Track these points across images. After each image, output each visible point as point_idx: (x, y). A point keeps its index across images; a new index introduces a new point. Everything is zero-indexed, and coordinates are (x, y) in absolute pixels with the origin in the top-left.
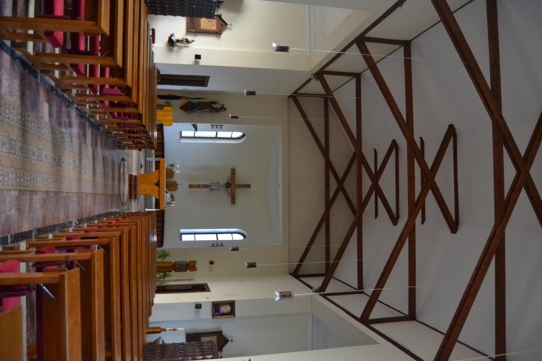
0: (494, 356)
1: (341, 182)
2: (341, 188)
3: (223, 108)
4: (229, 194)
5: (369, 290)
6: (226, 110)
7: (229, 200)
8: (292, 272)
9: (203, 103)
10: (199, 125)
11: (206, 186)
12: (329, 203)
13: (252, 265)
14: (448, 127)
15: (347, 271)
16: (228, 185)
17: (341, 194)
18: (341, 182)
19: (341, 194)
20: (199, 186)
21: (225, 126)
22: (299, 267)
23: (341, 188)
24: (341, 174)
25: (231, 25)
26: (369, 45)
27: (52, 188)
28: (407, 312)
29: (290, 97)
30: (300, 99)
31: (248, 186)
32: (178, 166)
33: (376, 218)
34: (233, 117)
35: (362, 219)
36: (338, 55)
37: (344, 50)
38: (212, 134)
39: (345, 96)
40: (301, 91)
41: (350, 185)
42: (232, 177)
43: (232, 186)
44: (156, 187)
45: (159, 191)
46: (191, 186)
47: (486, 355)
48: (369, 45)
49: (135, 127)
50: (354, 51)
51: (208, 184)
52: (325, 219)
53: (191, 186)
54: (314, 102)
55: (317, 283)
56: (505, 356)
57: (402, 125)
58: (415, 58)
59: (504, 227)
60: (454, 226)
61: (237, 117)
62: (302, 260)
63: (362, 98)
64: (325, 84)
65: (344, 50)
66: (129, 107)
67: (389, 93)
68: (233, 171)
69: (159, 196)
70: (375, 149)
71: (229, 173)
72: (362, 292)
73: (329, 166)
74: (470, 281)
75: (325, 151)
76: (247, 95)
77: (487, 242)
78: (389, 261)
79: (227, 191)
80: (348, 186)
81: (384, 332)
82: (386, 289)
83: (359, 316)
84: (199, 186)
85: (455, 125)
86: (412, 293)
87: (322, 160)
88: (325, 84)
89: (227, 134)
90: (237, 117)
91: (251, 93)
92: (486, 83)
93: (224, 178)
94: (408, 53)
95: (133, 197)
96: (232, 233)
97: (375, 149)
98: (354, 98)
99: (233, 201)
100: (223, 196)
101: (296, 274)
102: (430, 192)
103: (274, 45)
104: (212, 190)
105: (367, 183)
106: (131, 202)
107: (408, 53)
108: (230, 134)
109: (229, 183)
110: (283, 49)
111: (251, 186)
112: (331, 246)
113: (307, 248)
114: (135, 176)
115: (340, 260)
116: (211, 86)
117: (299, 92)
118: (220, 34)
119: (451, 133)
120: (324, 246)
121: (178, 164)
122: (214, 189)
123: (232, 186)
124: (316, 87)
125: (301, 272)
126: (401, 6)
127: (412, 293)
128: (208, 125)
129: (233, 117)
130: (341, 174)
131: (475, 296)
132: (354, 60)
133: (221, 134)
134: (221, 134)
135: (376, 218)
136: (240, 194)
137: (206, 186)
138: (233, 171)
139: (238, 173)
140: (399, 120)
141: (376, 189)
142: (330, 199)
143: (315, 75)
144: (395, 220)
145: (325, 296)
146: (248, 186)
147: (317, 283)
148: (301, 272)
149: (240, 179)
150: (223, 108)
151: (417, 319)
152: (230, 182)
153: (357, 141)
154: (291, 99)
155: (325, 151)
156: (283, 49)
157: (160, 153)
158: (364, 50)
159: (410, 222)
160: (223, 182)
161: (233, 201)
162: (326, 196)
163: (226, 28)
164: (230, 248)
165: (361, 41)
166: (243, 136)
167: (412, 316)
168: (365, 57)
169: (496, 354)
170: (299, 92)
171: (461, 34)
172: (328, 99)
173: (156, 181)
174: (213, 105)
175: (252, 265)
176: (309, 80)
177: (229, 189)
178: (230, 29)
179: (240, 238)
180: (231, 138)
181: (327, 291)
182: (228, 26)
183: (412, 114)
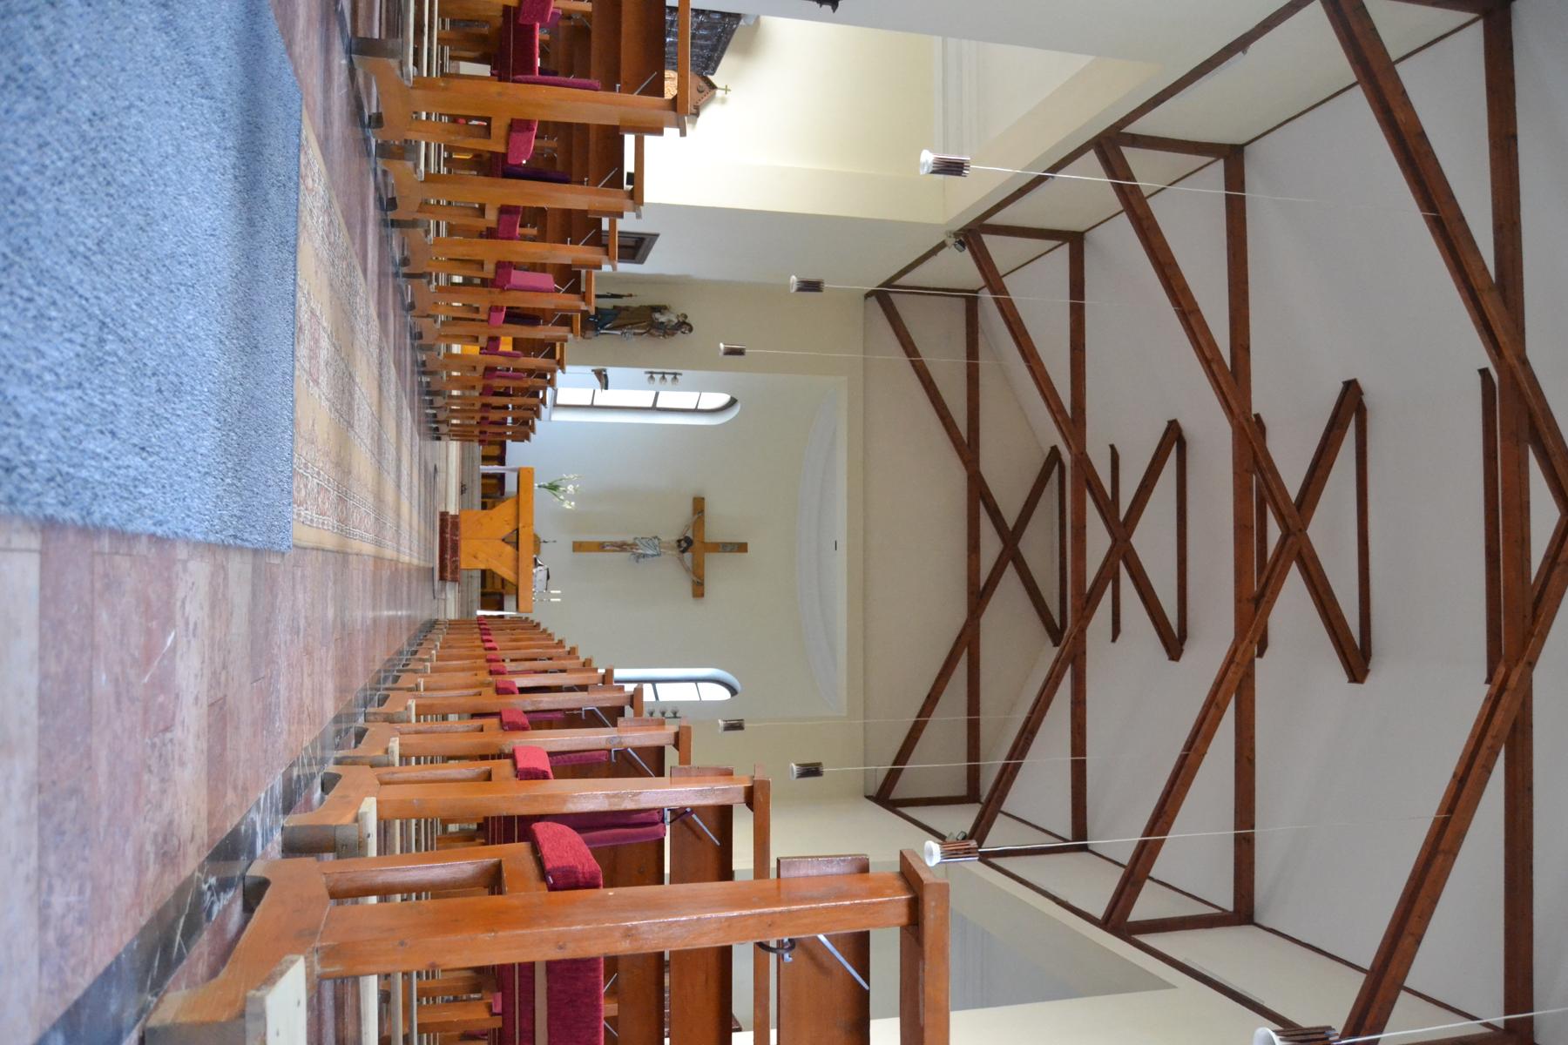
0: (1499, 1019)
1: (1011, 538)
2: (1011, 554)
3: (683, 325)
4: (687, 570)
5: (1118, 836)
6: (691, 330)
7: (687, 587)
8: (873, 791)
9: (627, 309)
10: (612, 372)
11: (622, 547)
12: (979, 597)
13: (811, 771)
14: (1340, 386)
15: (1040, 792)
16: (685, 544)
17: (1010, 571)
18: (1011, 538)
19: (1010, 571)
20: (601, 547)
21: (687, 375)
22: (893, 777)
23: (1011, 554)
24: (1011, 519)
25: (726, 90)
26: (1132, 155)
27: (329, 540)
28: (1229, 905)
29: (868, 295)
30: (900, 302)
31: (742, 547)
32: (570, 488)
33: (1114, 640)
34: (731, 352)
35: (1084, 641)
36: (1039, 180)
37: (1056, 168)
38: (646, 399)
39: (1039, 289)
40: (906, 280)
41: (1039, 547)
42: (695, 523)
43: (695, 547)
44: (509, 549)
45: (517, 559)
46: (578, 547)
47: (1473, 1018)
48: (1132, 155)
49: (520, 378)
50: (1090, 175)
51: (629, 539)
52: (968, 642)
53: (578, 547)
54: (942, 309)
55: (960, 820)
56: (1531, 1019)
57: (1221, 379)
58: (1256, 194)
59: (1531, 665)
60: (1356, 660)
61: (740, 352)
62: (903, 756)
63: (1088, 302)
64: (983, 261)
65: (1056, 168)
66: (546, 323)
67: (1185, 289)
68: (699, 505)
69: (517, 573)
70: (1112, 447)
71: (687, 508)
72: (1085, 848)
73: (979, 493)
74: (1439, 812)
75: (968, 449)
76: (799, 290)
77: (1483, 707)
78: (1183, 759)
79: (681, 560)
80: (1043, 548)
81: (1179, 957)
82: (1174, 837)
83: (1099, 913)
84: (601, 547)
85: (1362, 383)
86: (1244, 848)
87: (959, 475)
88: (983, 261)
89: (686, 399)
90: (740, 352)
91: (811, 286)
92: (1485, 268)
93: (674, 525)
94: (1235, 181)
95: (449, 576)
96: (696, 680)
97: (1112, 447)
98: (1065, 301)
99: (698, 590)
100: (671, 573)
101: (886, 797)
102: (1294, 568)
103: (928, 157)
104: (639, 557)
105: (1098, 541)
106: (443, 589)
107: (1235, 181)
108: (694, 398)
109: (689, 542)
110: (952, 168)
111: (749, 547)
112: (983, 718)
113: (916, 723)
114: (455, 517)
115: (1023, 757)
116: (655, 263)
117: (897, 283)
118: (697, 115)
119: (1351, 404)
120: (963, 717)
121: (570, 481)
122: (644, 556)
123: (695, 547)
124: (959, 268)
125: (896, 794)
126: (1244, 52)
127: (1244, 848)
128: (639, 373)
129: (731, 352)
130: (1011, 519)
131: (1455, 855)
132: (1085, 191)
133: (669, 399)
134: (669, 399)
135: (1114, 640)
136: (716, 566)
137: (622, 547)
138: (699, 505)
139: (711, 509)
140: (1215, 367)
141: (1122, 552)
142: (982, 585)
143: (956, 234)
144: (1174, 643)
145: (985, 858)
146: (742, 547)
147: (960, 820)
148: (896, 794)
149: (715, 531)
150: (683, 325)
151: (1257, 920)
152: (689, 534)
153: (1073, 423)
154: (873, 300)
155: (968, 449)
156: (952, 168)
157: (495, 451)
158: (1115, 167)
159: (1242, 648)
160: (671, 535)
161: (698, 590)
162: (969, 578)
163: (713, 97)
164: (721, 723)
165: (1110, 146)
166: (732, 402)
167: (1243, 913)
168: (1119, 189)
169: (1507, 1013)
170: (897, 283)
171: (1422, 135)
172: (983, 305)
173: (508, 530)
174: (657, 315)
175: (811, 771)
176: (942, 245)
177: (687, 555)
178: (723, 101)
179: (722, 694)
180: (696, 411)
181: (990, 844)
182: (719, 93)
183: (1247, 349)
